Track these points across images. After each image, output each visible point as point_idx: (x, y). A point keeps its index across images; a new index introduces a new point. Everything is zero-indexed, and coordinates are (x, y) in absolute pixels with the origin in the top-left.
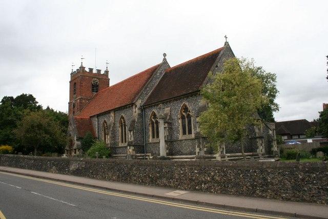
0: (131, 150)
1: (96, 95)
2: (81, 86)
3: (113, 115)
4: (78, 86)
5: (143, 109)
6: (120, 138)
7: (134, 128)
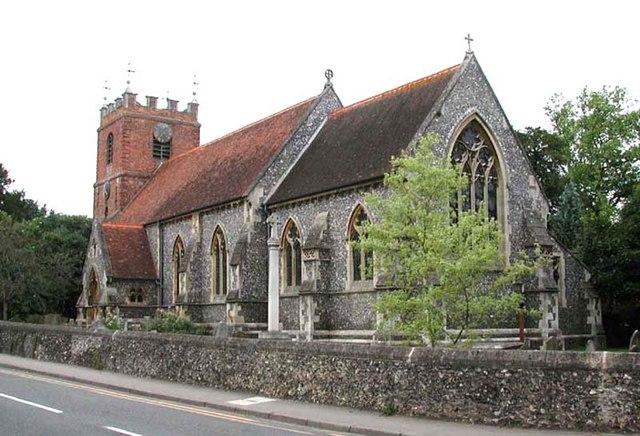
0: (233, 314)
1: (165, 167)
2: (126, 143)
3: (197, 225)
4: (117, 143)
5: (266, 210)
6: (212, 280)
7: (243, 258)
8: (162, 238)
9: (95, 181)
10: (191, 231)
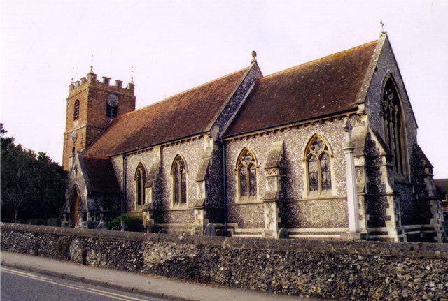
8: (125, 164)
10: (151, 159)
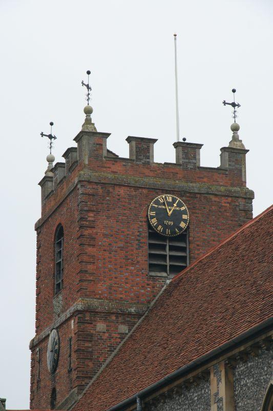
1: (174, 286)
3: (222, 393)
4: (70, 243)
9: (33, 335)
